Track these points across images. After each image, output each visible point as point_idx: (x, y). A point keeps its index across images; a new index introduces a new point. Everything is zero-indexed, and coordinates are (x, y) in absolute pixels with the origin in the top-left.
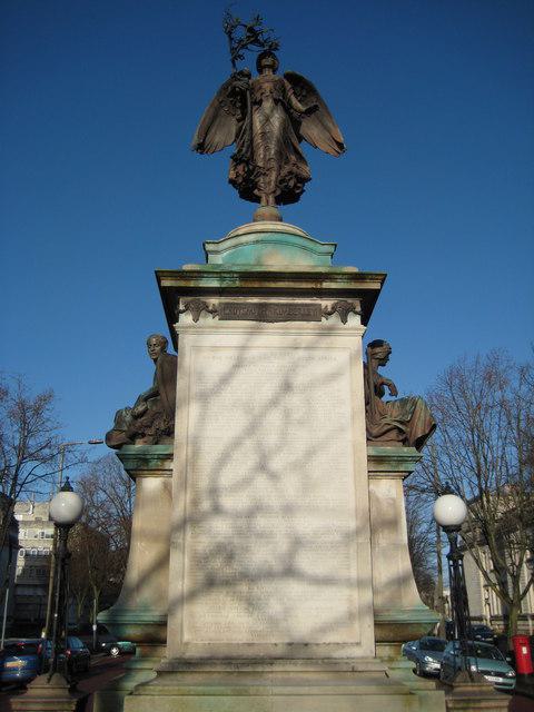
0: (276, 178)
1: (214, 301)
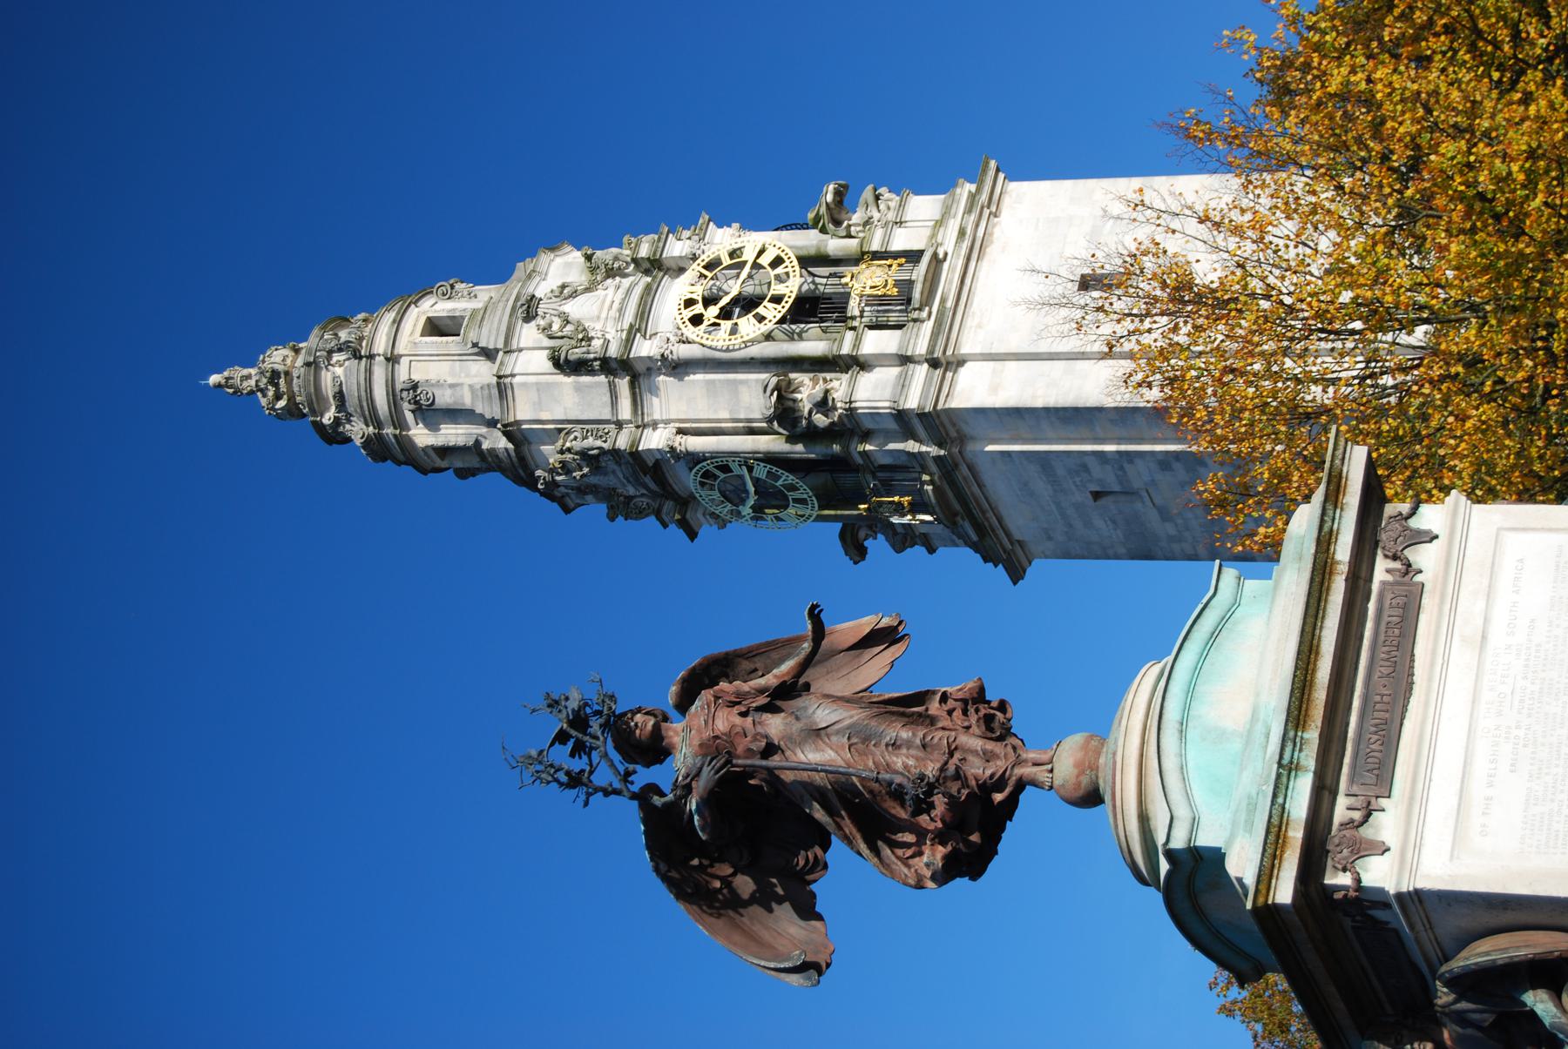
1: (1342, 810)
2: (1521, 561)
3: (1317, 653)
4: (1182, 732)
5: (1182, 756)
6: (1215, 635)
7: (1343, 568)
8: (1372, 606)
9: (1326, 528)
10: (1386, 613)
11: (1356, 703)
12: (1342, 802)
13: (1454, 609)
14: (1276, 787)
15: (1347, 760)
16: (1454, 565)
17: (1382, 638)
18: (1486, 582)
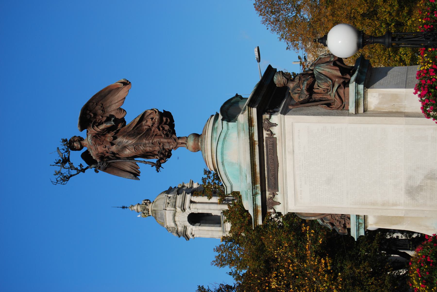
0: (165, 138)
1: (268, 194)
2: (299, 131)
3: (255, 165)
4: (223, 164)
5: (224, 170)
6: (224, 138)
7: (257, 142)
8: (265, 143)
9: (251, 134)
10: (268, 146)
11: (266, 169)
12: (267, 193)
13: (285, 145)
14: (253, 200)
15: (266, 183)
16: (283, 133)
17: (269, 153)
18: (291, 137)
